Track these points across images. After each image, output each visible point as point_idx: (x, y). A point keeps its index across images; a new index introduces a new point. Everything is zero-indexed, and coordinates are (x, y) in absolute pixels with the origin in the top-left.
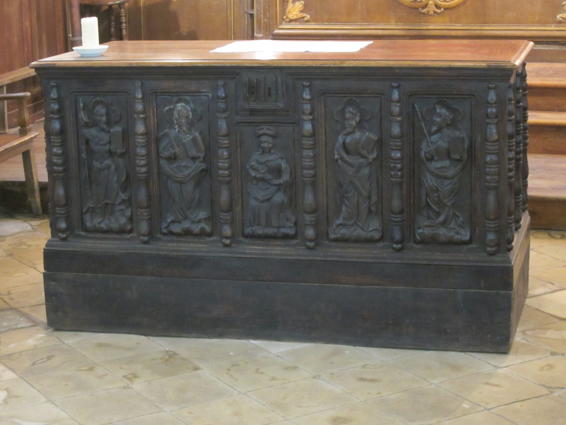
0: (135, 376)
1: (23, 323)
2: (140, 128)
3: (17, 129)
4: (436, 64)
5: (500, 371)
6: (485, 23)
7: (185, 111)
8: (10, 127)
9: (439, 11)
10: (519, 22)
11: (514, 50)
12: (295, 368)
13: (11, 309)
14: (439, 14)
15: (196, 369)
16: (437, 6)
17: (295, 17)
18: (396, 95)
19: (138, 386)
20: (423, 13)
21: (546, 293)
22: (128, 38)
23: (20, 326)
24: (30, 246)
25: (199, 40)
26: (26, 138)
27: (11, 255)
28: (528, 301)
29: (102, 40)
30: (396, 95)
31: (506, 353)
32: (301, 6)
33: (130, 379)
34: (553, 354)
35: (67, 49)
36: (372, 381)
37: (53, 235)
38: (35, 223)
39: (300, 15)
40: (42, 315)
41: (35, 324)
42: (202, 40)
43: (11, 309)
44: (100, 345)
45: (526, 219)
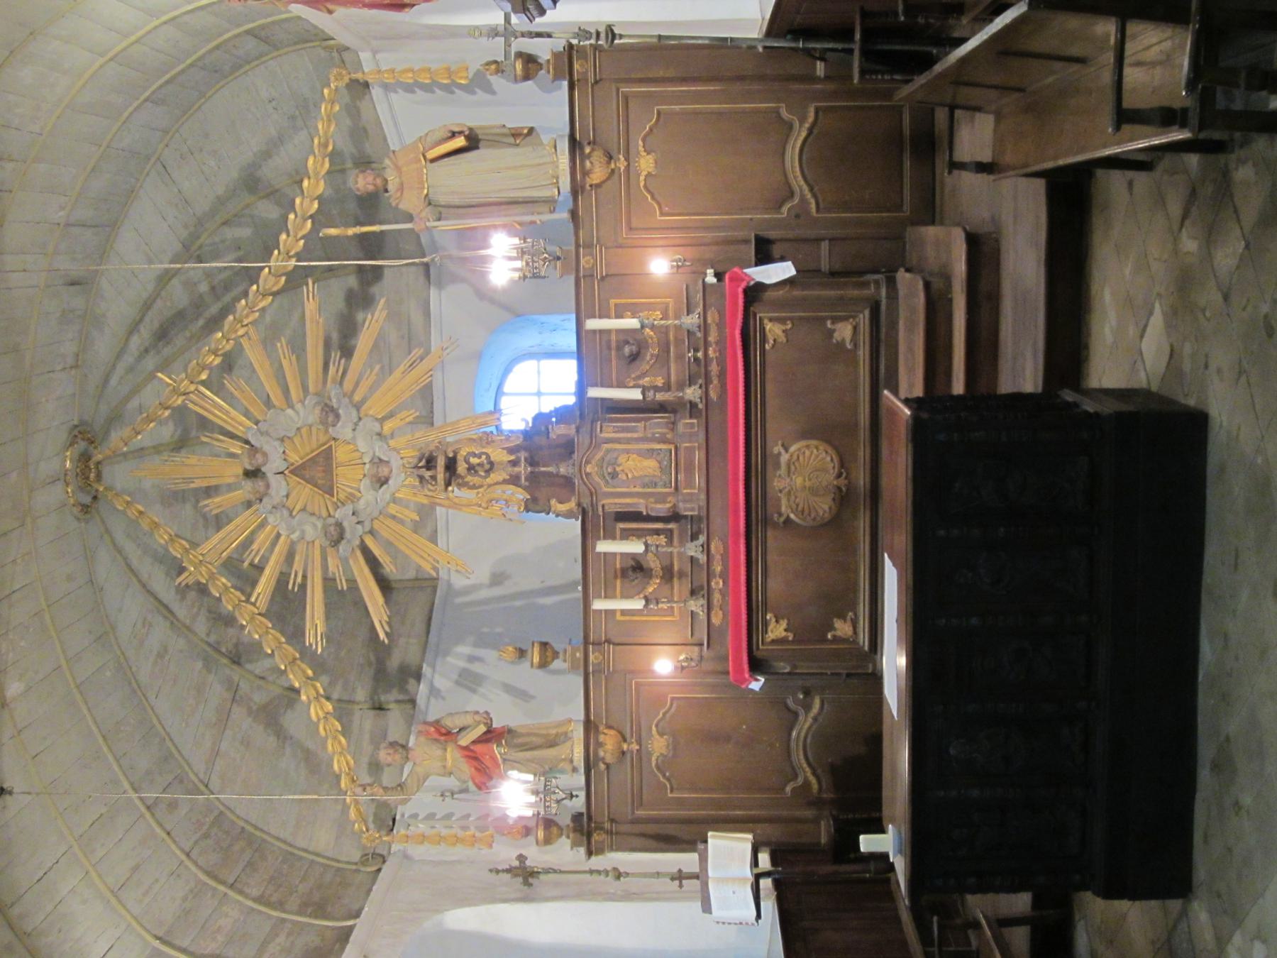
0: (1237, 803)
1: (1183, 926)
2: (975, 793)
3: (972, 935)
5: (1225, 424)
6: (856, 425)
8: (969, 944)
9: (844, 475)
10: (856, 388)
11: (893, 412)
12: (1226, 635)
13: (1169, 940)
14: (848, 474)
15: (1228, 739)
16: (839, 475)
17: (851, 628)
18: (942, 533)
19: (1247, 800)
20: (848, 490)
21: (1145, 370)
23: (1186, 929)
24: (1102, 922)
26: (984, 922)
27: (1111, 942)
28: (1154, 388)
29: (882, 830)
30: (942, 533)
31: (1197, 422)
33: (1240, 808)
34: (1206, 367)
35: (891, 867)
36: (1237, 557)
37: (1087, 889)
38: (1077, 917)
40: (1175, 905)
41: (1184, 913)
43: (1169, 940)
44: (1206, 841)
45: (1068, 396)
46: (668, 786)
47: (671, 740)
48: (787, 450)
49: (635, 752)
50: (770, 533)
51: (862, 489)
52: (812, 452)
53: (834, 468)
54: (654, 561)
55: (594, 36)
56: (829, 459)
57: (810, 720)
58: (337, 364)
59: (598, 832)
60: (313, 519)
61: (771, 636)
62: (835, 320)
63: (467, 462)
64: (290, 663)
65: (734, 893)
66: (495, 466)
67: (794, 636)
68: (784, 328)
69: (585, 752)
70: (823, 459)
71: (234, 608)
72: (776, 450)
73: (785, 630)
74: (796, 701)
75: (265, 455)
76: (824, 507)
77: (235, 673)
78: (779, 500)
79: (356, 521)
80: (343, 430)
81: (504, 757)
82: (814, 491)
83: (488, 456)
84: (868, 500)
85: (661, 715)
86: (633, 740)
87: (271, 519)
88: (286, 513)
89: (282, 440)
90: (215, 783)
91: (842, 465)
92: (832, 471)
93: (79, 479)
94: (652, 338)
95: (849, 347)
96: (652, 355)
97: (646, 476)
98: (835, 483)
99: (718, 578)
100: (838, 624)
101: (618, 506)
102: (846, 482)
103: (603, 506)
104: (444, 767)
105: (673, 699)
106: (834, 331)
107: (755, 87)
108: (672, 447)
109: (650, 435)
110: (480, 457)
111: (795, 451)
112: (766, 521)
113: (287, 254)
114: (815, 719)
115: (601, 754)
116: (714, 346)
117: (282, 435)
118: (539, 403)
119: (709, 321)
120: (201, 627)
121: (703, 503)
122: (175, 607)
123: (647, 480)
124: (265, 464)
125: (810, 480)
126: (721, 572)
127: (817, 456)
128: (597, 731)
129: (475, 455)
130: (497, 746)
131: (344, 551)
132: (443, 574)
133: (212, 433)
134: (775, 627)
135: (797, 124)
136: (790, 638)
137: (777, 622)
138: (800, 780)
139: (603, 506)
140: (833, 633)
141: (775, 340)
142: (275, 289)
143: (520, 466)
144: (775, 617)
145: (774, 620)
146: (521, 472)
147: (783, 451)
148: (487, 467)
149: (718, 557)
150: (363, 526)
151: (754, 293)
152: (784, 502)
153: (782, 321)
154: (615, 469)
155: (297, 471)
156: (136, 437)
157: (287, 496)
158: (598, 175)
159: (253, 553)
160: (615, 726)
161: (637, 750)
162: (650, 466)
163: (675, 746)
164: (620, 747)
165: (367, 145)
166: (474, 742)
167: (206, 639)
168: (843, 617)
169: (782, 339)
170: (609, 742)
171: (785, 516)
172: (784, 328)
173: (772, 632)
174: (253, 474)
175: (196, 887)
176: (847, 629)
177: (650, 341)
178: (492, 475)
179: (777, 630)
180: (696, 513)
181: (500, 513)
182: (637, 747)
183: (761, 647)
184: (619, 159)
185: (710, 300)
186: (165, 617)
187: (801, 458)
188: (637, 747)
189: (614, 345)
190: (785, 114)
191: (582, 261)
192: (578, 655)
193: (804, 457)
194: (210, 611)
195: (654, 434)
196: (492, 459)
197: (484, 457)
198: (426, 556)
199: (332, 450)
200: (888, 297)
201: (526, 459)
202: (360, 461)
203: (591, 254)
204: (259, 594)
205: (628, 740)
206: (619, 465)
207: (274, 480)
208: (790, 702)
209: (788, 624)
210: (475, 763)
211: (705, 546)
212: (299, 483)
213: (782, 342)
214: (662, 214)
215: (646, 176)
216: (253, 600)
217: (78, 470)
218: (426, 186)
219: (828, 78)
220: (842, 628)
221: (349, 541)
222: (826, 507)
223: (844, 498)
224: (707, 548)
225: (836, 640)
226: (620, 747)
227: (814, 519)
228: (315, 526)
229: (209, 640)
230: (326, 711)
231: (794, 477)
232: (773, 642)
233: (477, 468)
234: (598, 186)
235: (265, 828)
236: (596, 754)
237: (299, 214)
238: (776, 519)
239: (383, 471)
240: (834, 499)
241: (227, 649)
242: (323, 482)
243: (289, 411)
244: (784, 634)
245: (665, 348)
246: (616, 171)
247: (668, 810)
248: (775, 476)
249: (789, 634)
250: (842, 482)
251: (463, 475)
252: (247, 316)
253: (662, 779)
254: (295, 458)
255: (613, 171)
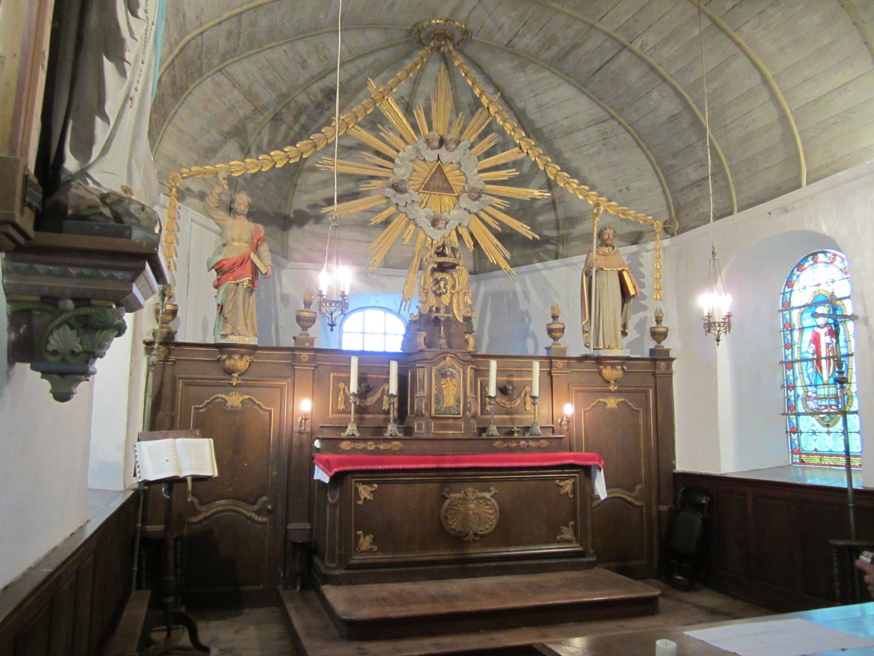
4: (82, 311)
7: (810, 448)
9: (477, 538)
16: (476, 535)
17: (366, 549)
20: (466, 541)
22: (534, 645)
25: (43, 231)
32: (371, 539)
39: (370, 547)
42: (482, 631)
46: (201, 406)
47: (239, 409)
48: (492, 496)
49: (231, 382)
50: (436, 485)
51: (467, 552)
52: (492, 514)
53: (482, 531)
54: (372, 401)
55: (840, 370)
56: (487, 527)
57: (249, 514)
58: (503, 204)
59: (167, 350)
60: (408, 175)
61: (361, 488)
62: (575, 528)
63: (441, 279)
64: (315, 143)
65: (167, 461)
66: (438, 298)
67: (360, 505)
68: (569, 492)
69: (239, 344)
70: (487, 523)
71: (354, 112)
72: (492, 488)
73: (365, 498)
74: (266, 502)
75: (453, 150)
76: (454, 525)
77: (269, 115)
78: (459, 492)
79: (408, 202)
80: (465, 202)
81: (241, 285)
82: (465, 517)
83: (444, 293)
84: (461, 556)
85: (258, 402)
86: (240, 381)
87: (409, 147)
88: (413, 157)
89: (459, 163)
90: (220, 78)
91: (482, 536)
92: (479, 530)
93: (443, 31)
94: (515, 403)
95: (558, 537)
96: (505, 404)
97: (444, 397)
98: (471, 532)
99: (375, 446)
100: (369, 539)
101: (422, 378)
102: (471, 540)
103: (423, 367)
104: (234, 240)
105: (270, 412)
106: (568, 527)
107: (654, 469)
108: (461, 416)
109: (468, 400)
110: (444, 288)
111: (492, 502)
112: (445, 483)
113: (567, 183)
114: (250, 518)
115: (236, 357)
116: (527, 444)
117: (462, 164)
118: (364, 337)
119: (542, 441)
120: (302, 98)
121: (421, 437)
122: (320, 84)
123: (441, 398)
124: (447, 149)
125: (473, 514)
126: (379, 449)
127: (489, 518)
128: (250, 354)
129: (445, 285)
130: (249, 280)
131: (388, 192)
132: (291, 264)
133: (464, 121)
134: (368, 491)
135: (634, 494)
136: (358, 502)
137: (372, 492)
138: (198, 507)
139: (423, 367)
140: (362, 535)
141: (562, 487)
142: (548, 172)
143: (444, 313)
144: (375, 490)
145: (373, 489)
146: (440, 313)
147: (492, 493)
148: (438, 292)
149: (389, 446)
150: (403, 207)
151: (587, 471)
152: (458, 495)
153: (574, 491)
154: (449, 376)
155: (440, 169)
156: (463, 72)
157: (424, 160)
158: (607, 372)
159: (387, 133)
160: (250, 368)
161: (232, 384)
162: (450, 400)
163: (233, 412)
164: (237, 371)
165: (578, 243)
166: (252, 261)
167: (294, 100)
168: (374, 541)
169: (563, 491)
170: (241, 363)
171: (447, 496)
172: (569, 492)
173: (364, 488)
174: (442, 142)
175: (185, 29)
176: (365, 545)
177: (513, 402)
178: (433, 295)
179: (365, 492)
180: (416, 431)
181: (407, 298)
182: (234, 384)
183: (353, 480)
184: (615, 386)
185: (555, 443)
186: (320, 74)
187: (487, 507)
188: (234, 384)
189: (510, 379)
190: (638, 487)
191: (559, 361)
192: (307, 344)
193: (488, 509)
194: (307, 107)
195: (470, 403)
196: (442, 296)
197: (444, 290)
198: (381, 245)
199: (452, 193)
200: (589, 562)
201: (449, 317)
202: (443, 211)
203: (564, 367)
204: (360, 131)
205: (240, 378)
206: (451, 379)
207: (434, 153)
208: (264, 498)
209: (369, 500)
210: (239, 262)
211: (352, 437)
212: (431, 170)
213: (560, 491)
214: (585, 412)
215: (605, 403)
216: (356, 127)
217: (447, 32)
218: (608, 269)
219: (659, 512)
220: (366, 542)
221: (395, 196)
222: (454, 526)
223: (458, 540)
224: (394, 439)
225: (357, 537)
226: (237, 371)
227: (446, 518)
228: (405, 175)
229: (293, 102)
230: (278, 162)
231: (475, 502)
232: (357, 489)
233: (437, 285)
234: (600, 373)
235: (183, 106)
236: (235, 353)
237: (588, 193)
238: (445, 490)
239: (442, 224)
240: (460, 532)
241: (283, 113)
242: (432, 185)
243: (476, 171)
244: (362, 497)
245: (509, 412)
246: (608, 384)
247: (181, 407)
248: (475, 488)
249: (362, 501)
250: (471, 537)
251: (434, 276)
252: (533, 153)
253: (206, 401)
254: (446, 170)
255: (608, 382)
